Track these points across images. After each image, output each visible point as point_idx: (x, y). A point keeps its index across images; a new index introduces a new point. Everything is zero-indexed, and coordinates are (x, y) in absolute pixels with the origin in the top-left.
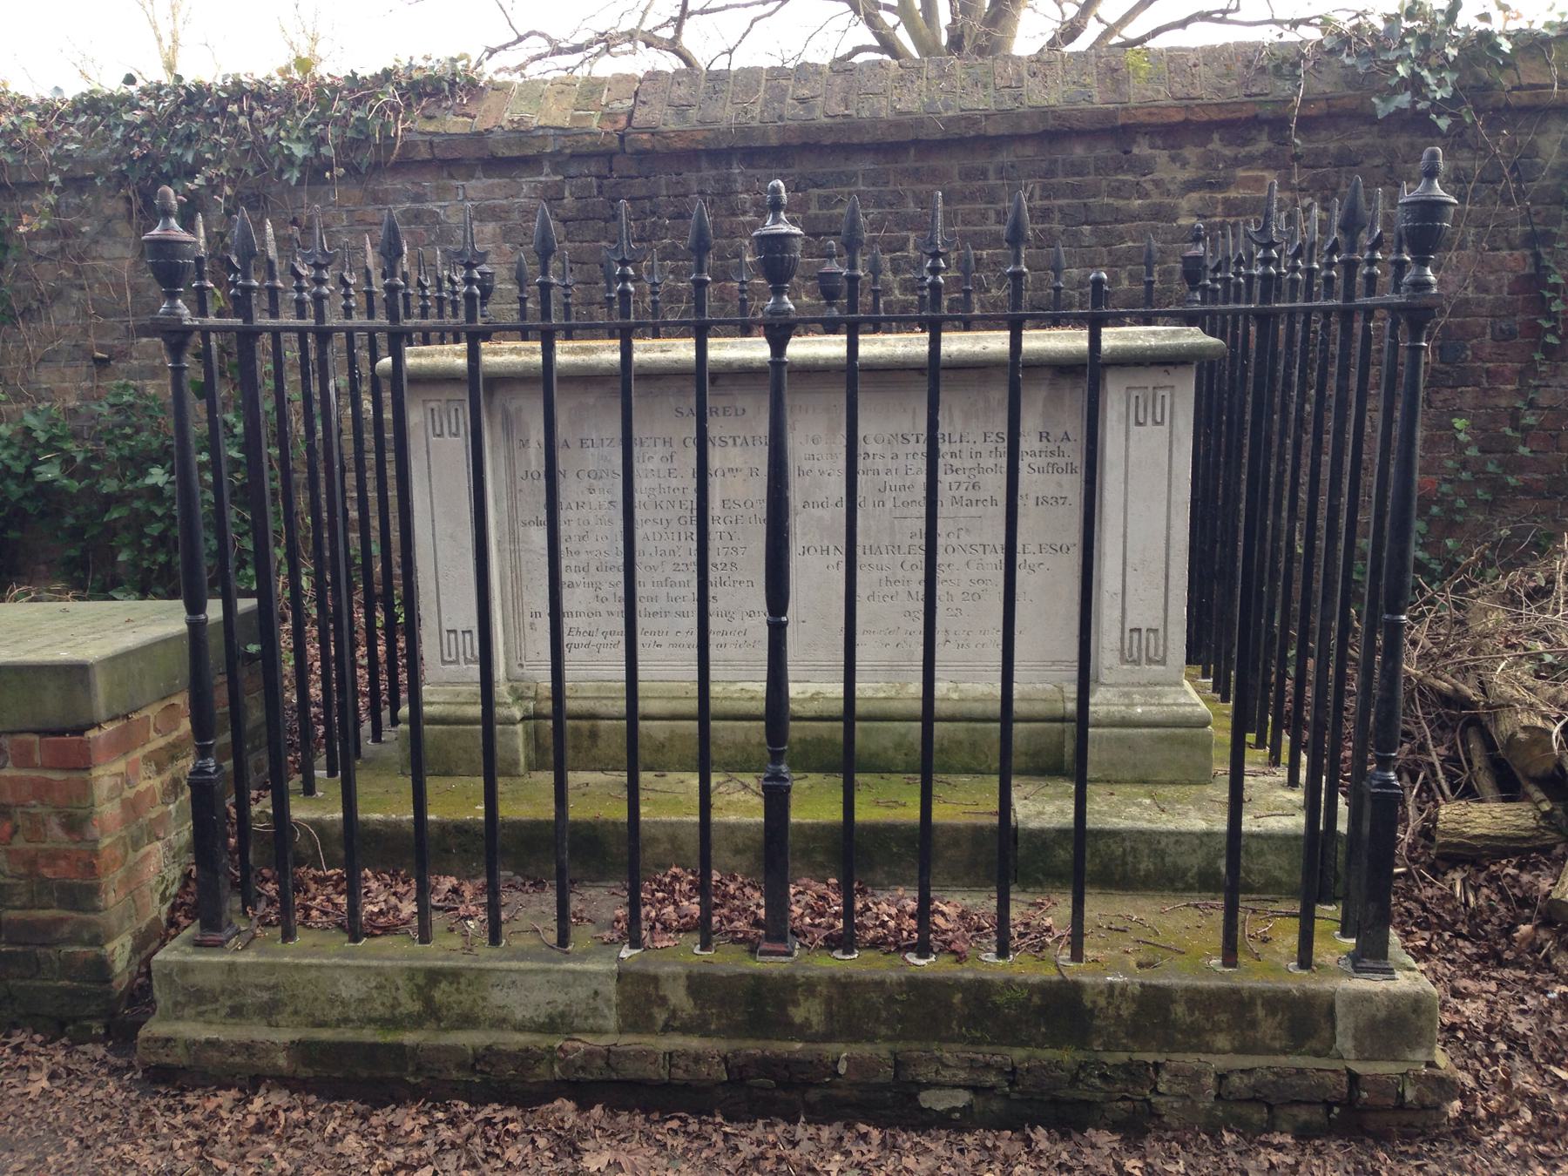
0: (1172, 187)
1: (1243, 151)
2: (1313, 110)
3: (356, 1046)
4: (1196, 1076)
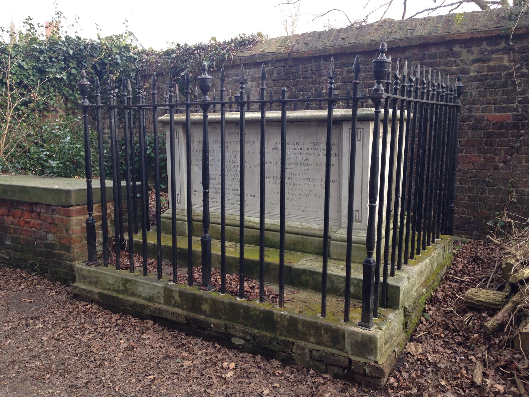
0: (468, 62)
1: (495, 48)
2: (521, 32)
3: (111, 296)
4: (303, 349)
